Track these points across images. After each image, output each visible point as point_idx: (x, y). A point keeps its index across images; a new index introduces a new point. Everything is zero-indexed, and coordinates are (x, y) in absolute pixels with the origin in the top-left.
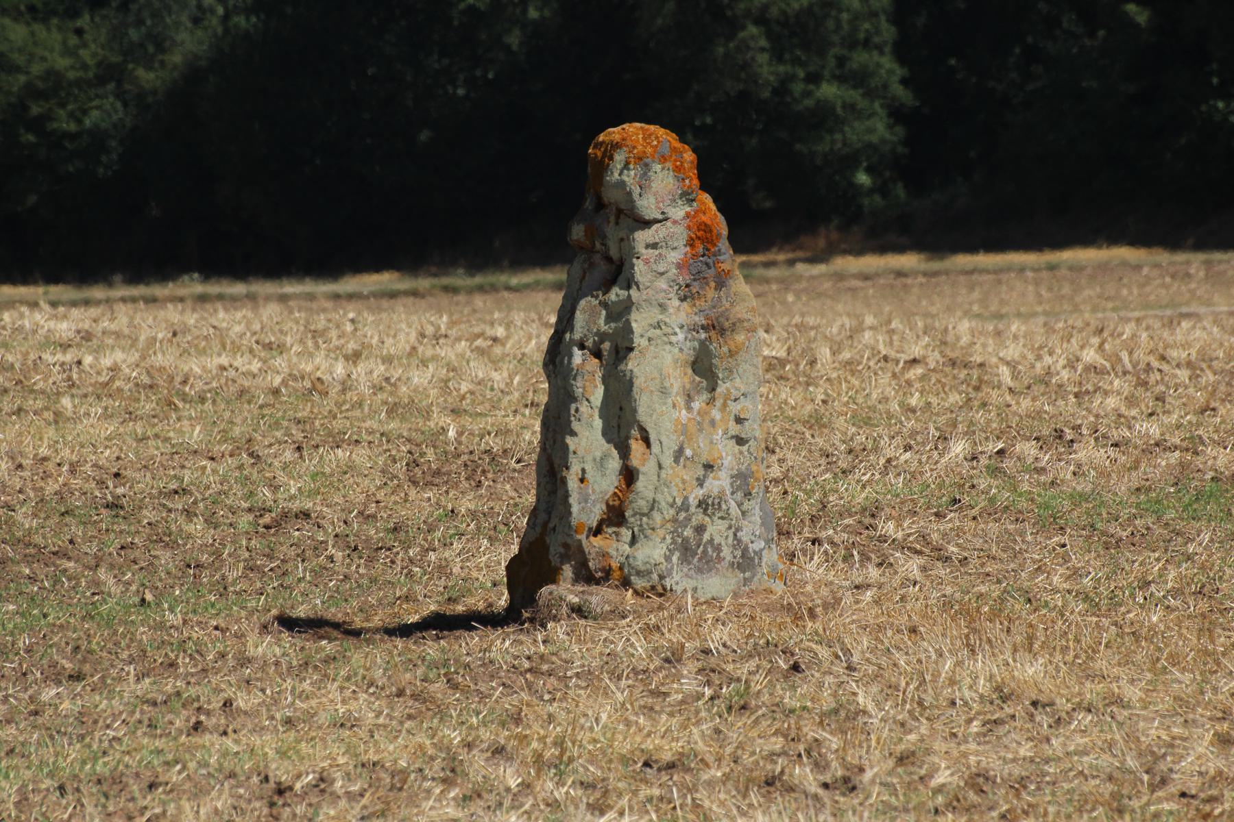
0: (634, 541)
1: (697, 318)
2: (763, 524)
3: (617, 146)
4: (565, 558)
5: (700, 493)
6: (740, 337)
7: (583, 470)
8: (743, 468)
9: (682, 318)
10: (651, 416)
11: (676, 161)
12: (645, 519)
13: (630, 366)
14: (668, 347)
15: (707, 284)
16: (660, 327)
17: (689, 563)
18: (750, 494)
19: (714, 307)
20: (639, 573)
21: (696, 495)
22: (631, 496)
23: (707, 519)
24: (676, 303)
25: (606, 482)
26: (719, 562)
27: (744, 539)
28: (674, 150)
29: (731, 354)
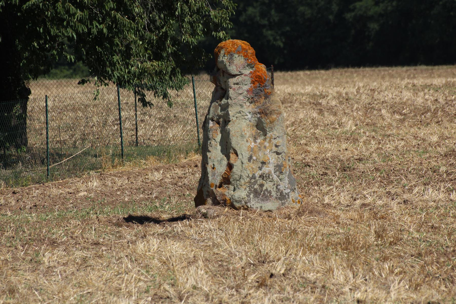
0: (234, 190)
1: (256, 110)
2: (289, 183)
3: (222, 48)
4: (208, 196)
5: (260, 172)
6: (274, 116)
7: (214, 165)
8: (280, 163)
9: (250, 109)
10: (238, 145)
11: (244, 53)
12: (238, 182)
13: (229, 127)
14: (244, 120)
15: (261, 97)
16: (240, 113)
17: (258, 198)
18: (282, 172)
19: (263, 106)
20: (236, 201)
21: (257, 174)
22: (232, 174)
23: (264, 182)
24: (248, 104)
25: (222, 169)
26: (271, 197)
27: (281, 189)
28: (244, 49)
29: (271, 122)
